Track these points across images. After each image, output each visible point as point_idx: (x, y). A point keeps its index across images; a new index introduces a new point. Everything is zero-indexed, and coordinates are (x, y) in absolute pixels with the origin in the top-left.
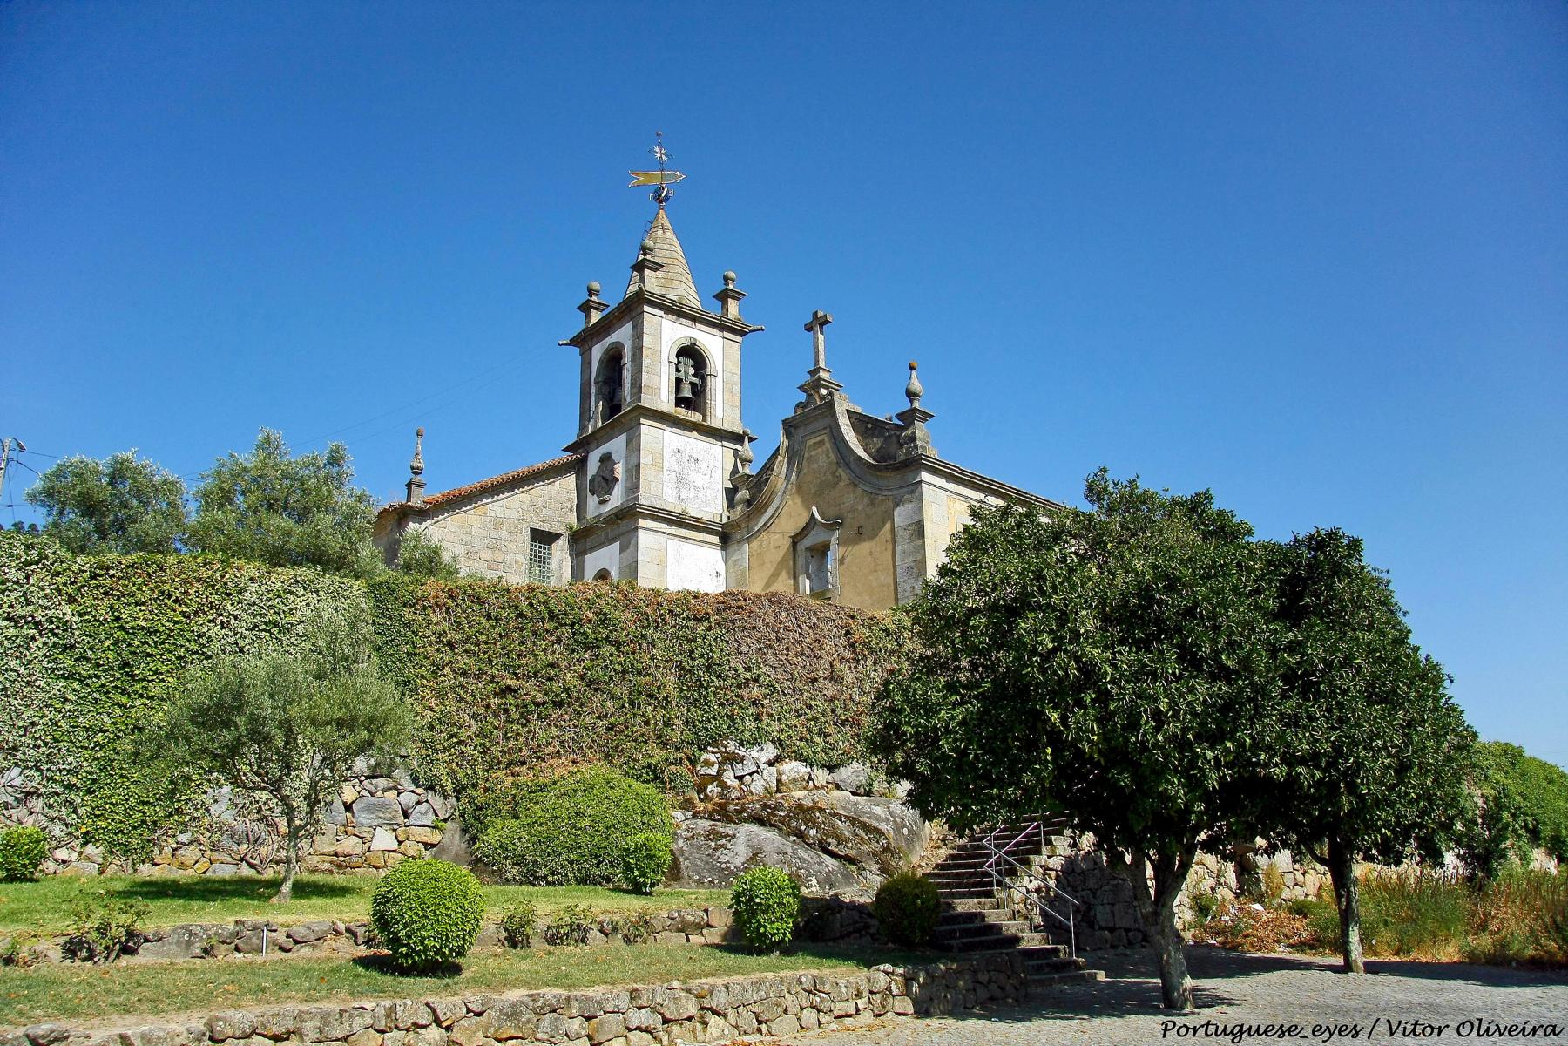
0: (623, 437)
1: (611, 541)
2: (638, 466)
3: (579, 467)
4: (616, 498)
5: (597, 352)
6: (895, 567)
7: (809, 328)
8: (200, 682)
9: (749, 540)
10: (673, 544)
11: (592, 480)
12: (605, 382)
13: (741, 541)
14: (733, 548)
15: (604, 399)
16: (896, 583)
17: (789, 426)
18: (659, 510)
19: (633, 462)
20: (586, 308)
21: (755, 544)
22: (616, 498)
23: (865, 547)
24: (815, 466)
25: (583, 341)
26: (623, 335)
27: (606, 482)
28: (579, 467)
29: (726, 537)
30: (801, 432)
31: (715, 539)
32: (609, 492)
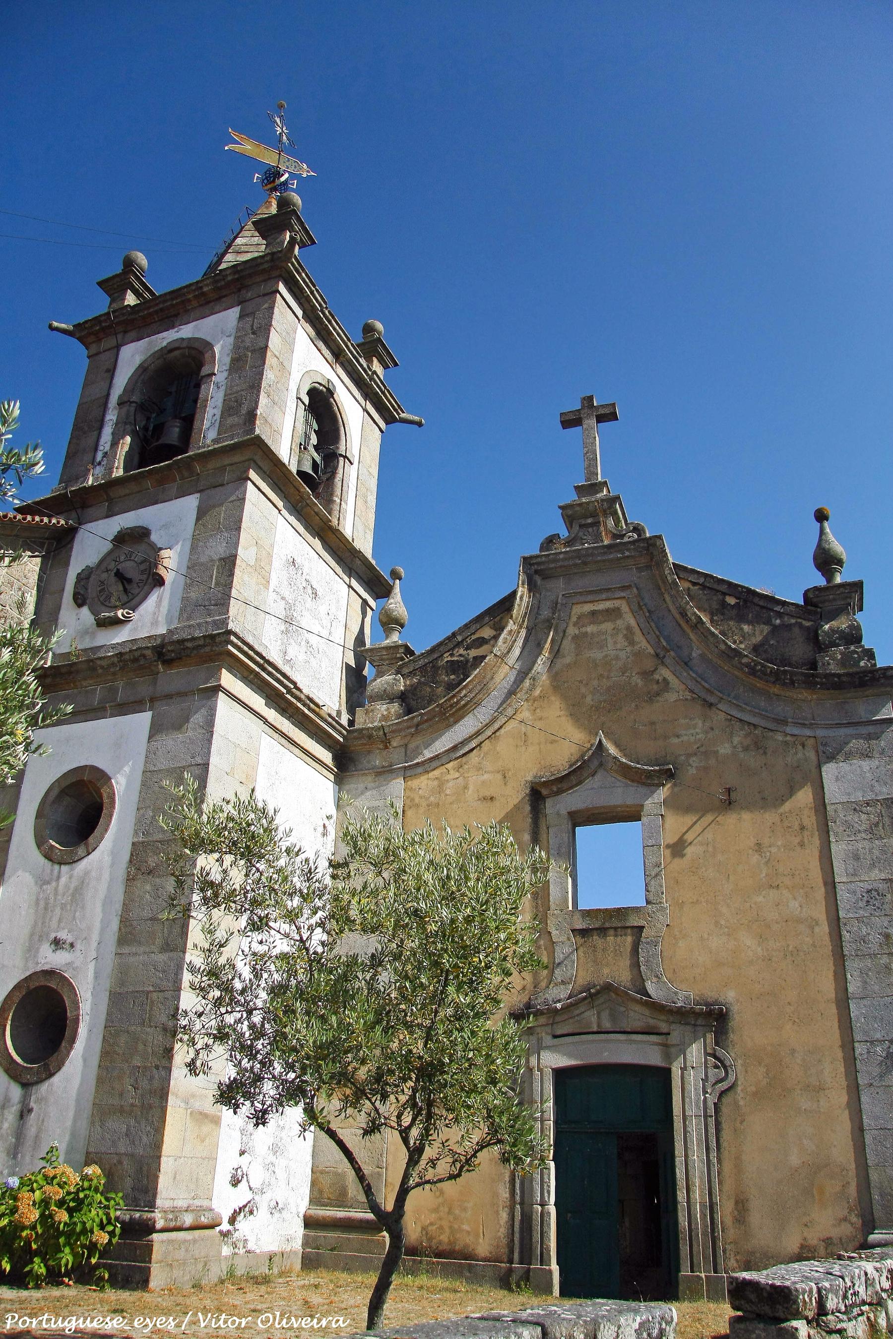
0: (191, 503)
1: (124, 708)
2: (229, 563)
3: (55, 547)
4: (152, 618)
5: (132, 356)
6: (831, 885)
7: (570, 421)
8: (323, 864)
9: (409, 772)
10: (269, 745)
11: (83, 578)
12: (142, 407)
13: (385, 772)
14: (355, 784)
15: (134, 434)
16: (836, 923)
17: (536, 571)
18: (267, 663)
19: (217, 549)
20: (114, 286)
21: (424, 783)
22: (152, 618)
23: (743, 826)
24: (597, 655)
25: (100, 335)
26: (218, 330)
27: (129, 574)
28: (55, 547)
29: (347, 759)
30: (558, 588)
31: (326, 756)
32: (133, 602)
